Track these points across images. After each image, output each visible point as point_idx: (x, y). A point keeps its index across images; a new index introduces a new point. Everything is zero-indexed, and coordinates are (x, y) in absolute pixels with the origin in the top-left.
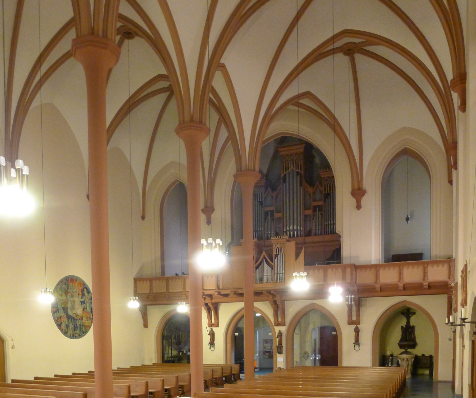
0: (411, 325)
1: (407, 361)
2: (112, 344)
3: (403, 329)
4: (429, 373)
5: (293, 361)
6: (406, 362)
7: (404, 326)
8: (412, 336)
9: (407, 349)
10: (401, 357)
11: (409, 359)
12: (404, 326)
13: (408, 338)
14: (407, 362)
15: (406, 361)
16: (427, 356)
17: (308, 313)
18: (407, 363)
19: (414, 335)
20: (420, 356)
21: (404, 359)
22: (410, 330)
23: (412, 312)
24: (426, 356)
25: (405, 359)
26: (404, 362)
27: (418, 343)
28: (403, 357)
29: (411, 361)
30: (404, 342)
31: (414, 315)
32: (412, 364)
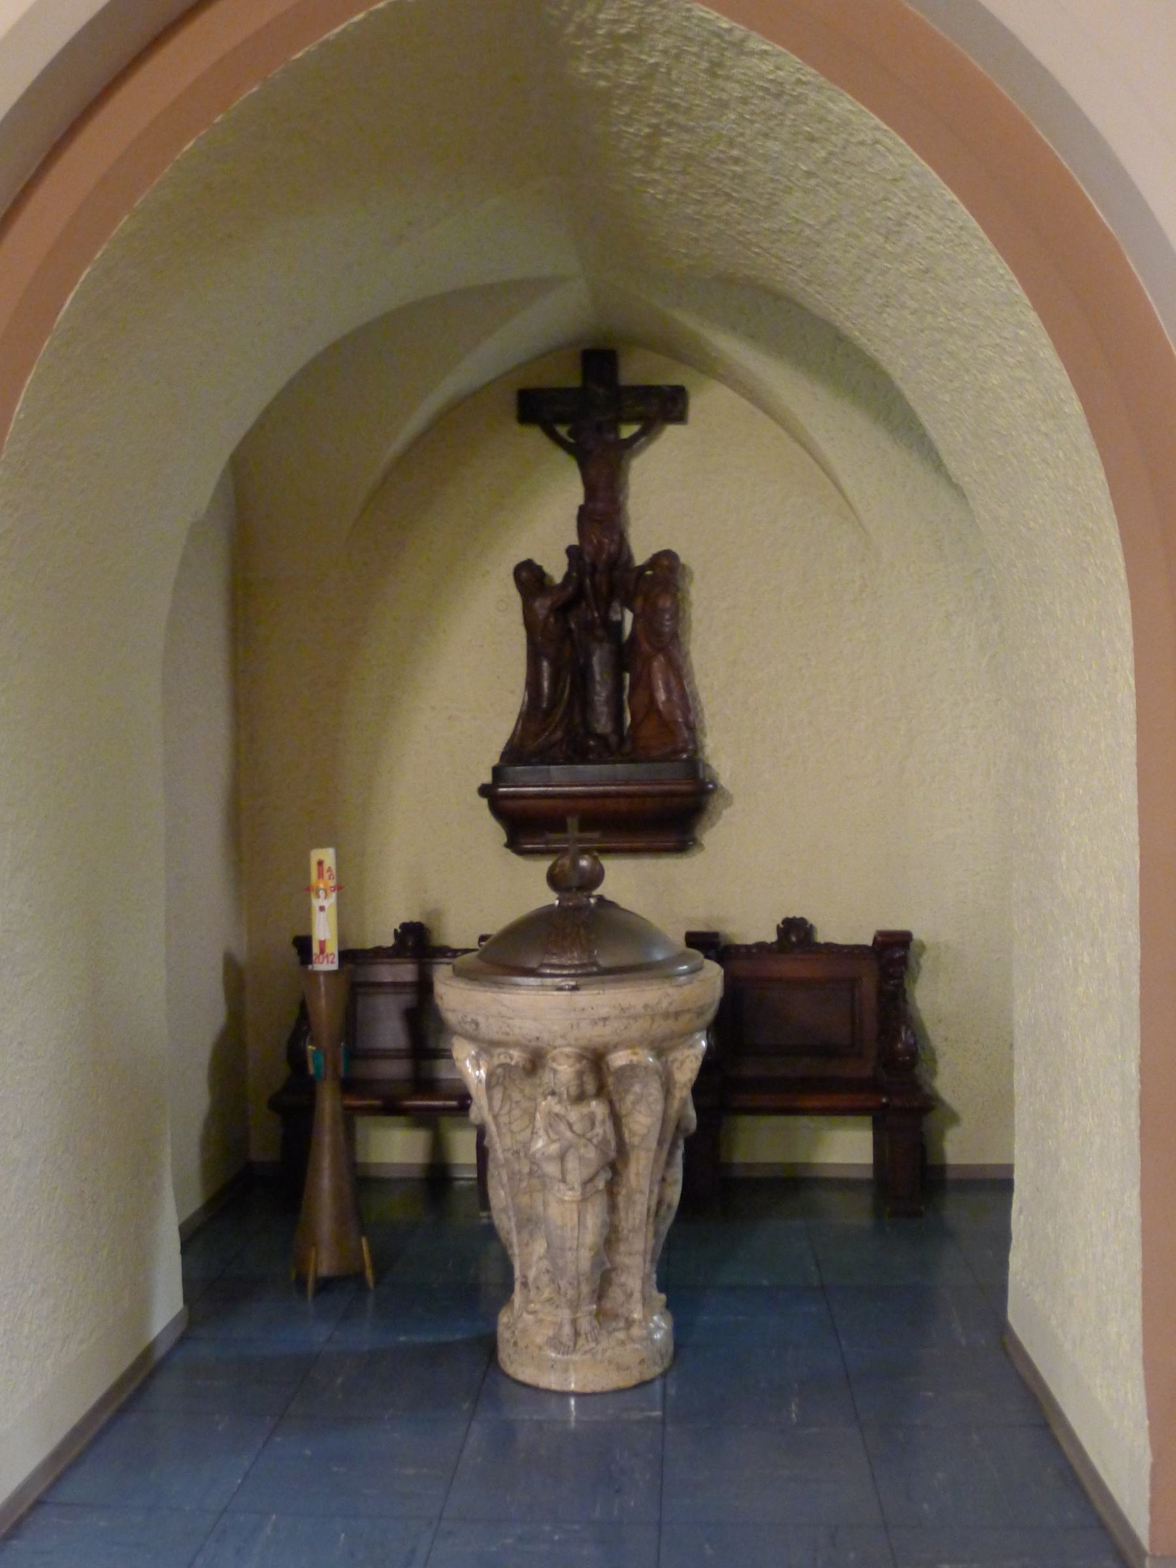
0: (641, 554)
1: (601, 1091)
2: (1128, 795)
3: (542, 606)
4: (874, 1161)
5: (339, 888)
6: (574, 1114)
7: (556, 568)
8: (661, 696)
9: (632, 610)
10: (491, 1029)
11: (619, 1059)
12: (556, 568)
13: (603, 725)
14: (597, 1108)
15: (580, 1098)
16: (840, 939)
17: (572, 822)
18: (603, 1129)
19: (678, 671)
20: (761, 946)
21: (536, 1062)
22: (629, 616)
23: (646, 392)
24: (832, 949)
25: (564, 1071)
26: (549, 1104)
27: (724, 780)
28: (526, 1028)
29: (655, 1090)
30: (557, 771)
31: (672, 432)
32: (670, 1130)
